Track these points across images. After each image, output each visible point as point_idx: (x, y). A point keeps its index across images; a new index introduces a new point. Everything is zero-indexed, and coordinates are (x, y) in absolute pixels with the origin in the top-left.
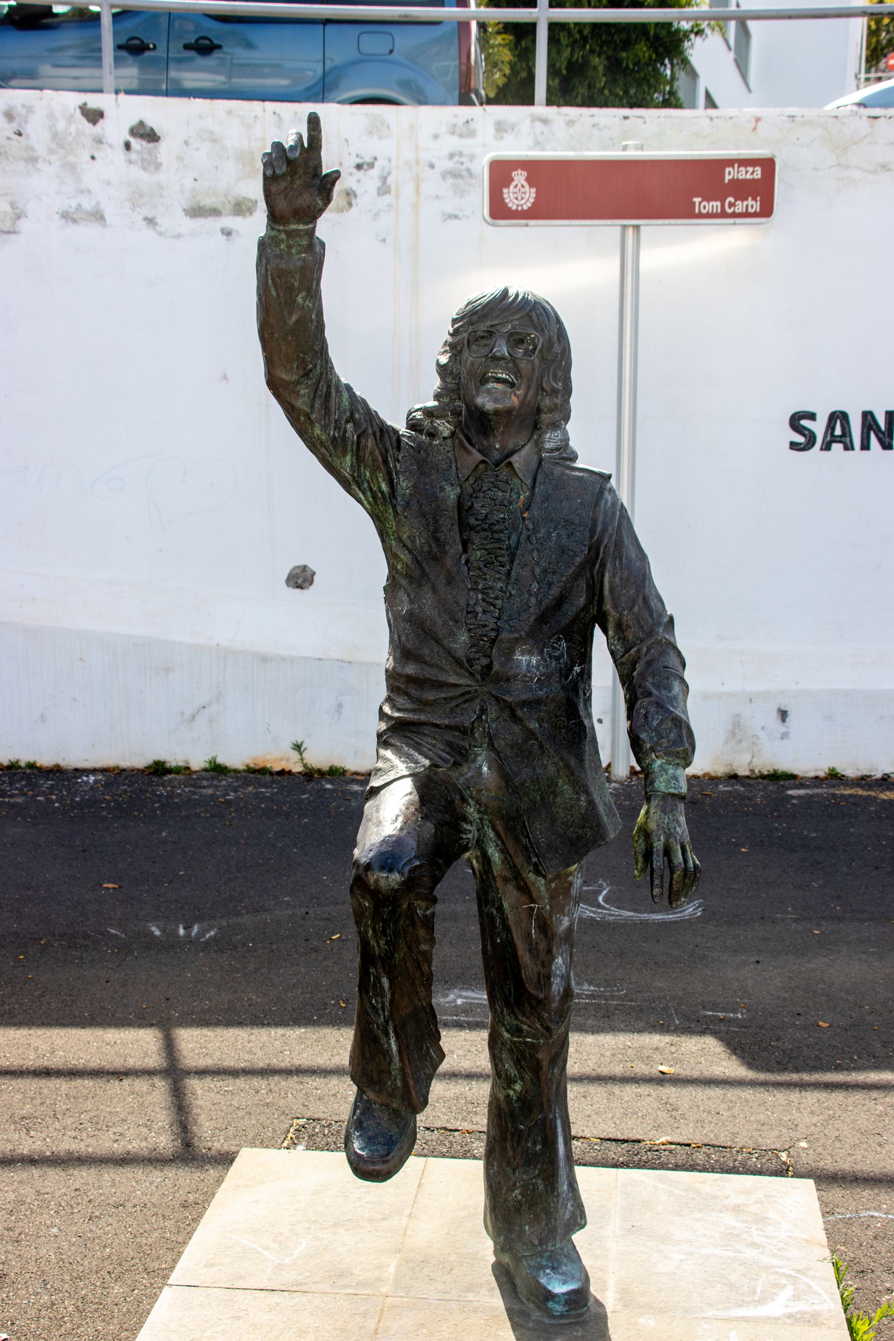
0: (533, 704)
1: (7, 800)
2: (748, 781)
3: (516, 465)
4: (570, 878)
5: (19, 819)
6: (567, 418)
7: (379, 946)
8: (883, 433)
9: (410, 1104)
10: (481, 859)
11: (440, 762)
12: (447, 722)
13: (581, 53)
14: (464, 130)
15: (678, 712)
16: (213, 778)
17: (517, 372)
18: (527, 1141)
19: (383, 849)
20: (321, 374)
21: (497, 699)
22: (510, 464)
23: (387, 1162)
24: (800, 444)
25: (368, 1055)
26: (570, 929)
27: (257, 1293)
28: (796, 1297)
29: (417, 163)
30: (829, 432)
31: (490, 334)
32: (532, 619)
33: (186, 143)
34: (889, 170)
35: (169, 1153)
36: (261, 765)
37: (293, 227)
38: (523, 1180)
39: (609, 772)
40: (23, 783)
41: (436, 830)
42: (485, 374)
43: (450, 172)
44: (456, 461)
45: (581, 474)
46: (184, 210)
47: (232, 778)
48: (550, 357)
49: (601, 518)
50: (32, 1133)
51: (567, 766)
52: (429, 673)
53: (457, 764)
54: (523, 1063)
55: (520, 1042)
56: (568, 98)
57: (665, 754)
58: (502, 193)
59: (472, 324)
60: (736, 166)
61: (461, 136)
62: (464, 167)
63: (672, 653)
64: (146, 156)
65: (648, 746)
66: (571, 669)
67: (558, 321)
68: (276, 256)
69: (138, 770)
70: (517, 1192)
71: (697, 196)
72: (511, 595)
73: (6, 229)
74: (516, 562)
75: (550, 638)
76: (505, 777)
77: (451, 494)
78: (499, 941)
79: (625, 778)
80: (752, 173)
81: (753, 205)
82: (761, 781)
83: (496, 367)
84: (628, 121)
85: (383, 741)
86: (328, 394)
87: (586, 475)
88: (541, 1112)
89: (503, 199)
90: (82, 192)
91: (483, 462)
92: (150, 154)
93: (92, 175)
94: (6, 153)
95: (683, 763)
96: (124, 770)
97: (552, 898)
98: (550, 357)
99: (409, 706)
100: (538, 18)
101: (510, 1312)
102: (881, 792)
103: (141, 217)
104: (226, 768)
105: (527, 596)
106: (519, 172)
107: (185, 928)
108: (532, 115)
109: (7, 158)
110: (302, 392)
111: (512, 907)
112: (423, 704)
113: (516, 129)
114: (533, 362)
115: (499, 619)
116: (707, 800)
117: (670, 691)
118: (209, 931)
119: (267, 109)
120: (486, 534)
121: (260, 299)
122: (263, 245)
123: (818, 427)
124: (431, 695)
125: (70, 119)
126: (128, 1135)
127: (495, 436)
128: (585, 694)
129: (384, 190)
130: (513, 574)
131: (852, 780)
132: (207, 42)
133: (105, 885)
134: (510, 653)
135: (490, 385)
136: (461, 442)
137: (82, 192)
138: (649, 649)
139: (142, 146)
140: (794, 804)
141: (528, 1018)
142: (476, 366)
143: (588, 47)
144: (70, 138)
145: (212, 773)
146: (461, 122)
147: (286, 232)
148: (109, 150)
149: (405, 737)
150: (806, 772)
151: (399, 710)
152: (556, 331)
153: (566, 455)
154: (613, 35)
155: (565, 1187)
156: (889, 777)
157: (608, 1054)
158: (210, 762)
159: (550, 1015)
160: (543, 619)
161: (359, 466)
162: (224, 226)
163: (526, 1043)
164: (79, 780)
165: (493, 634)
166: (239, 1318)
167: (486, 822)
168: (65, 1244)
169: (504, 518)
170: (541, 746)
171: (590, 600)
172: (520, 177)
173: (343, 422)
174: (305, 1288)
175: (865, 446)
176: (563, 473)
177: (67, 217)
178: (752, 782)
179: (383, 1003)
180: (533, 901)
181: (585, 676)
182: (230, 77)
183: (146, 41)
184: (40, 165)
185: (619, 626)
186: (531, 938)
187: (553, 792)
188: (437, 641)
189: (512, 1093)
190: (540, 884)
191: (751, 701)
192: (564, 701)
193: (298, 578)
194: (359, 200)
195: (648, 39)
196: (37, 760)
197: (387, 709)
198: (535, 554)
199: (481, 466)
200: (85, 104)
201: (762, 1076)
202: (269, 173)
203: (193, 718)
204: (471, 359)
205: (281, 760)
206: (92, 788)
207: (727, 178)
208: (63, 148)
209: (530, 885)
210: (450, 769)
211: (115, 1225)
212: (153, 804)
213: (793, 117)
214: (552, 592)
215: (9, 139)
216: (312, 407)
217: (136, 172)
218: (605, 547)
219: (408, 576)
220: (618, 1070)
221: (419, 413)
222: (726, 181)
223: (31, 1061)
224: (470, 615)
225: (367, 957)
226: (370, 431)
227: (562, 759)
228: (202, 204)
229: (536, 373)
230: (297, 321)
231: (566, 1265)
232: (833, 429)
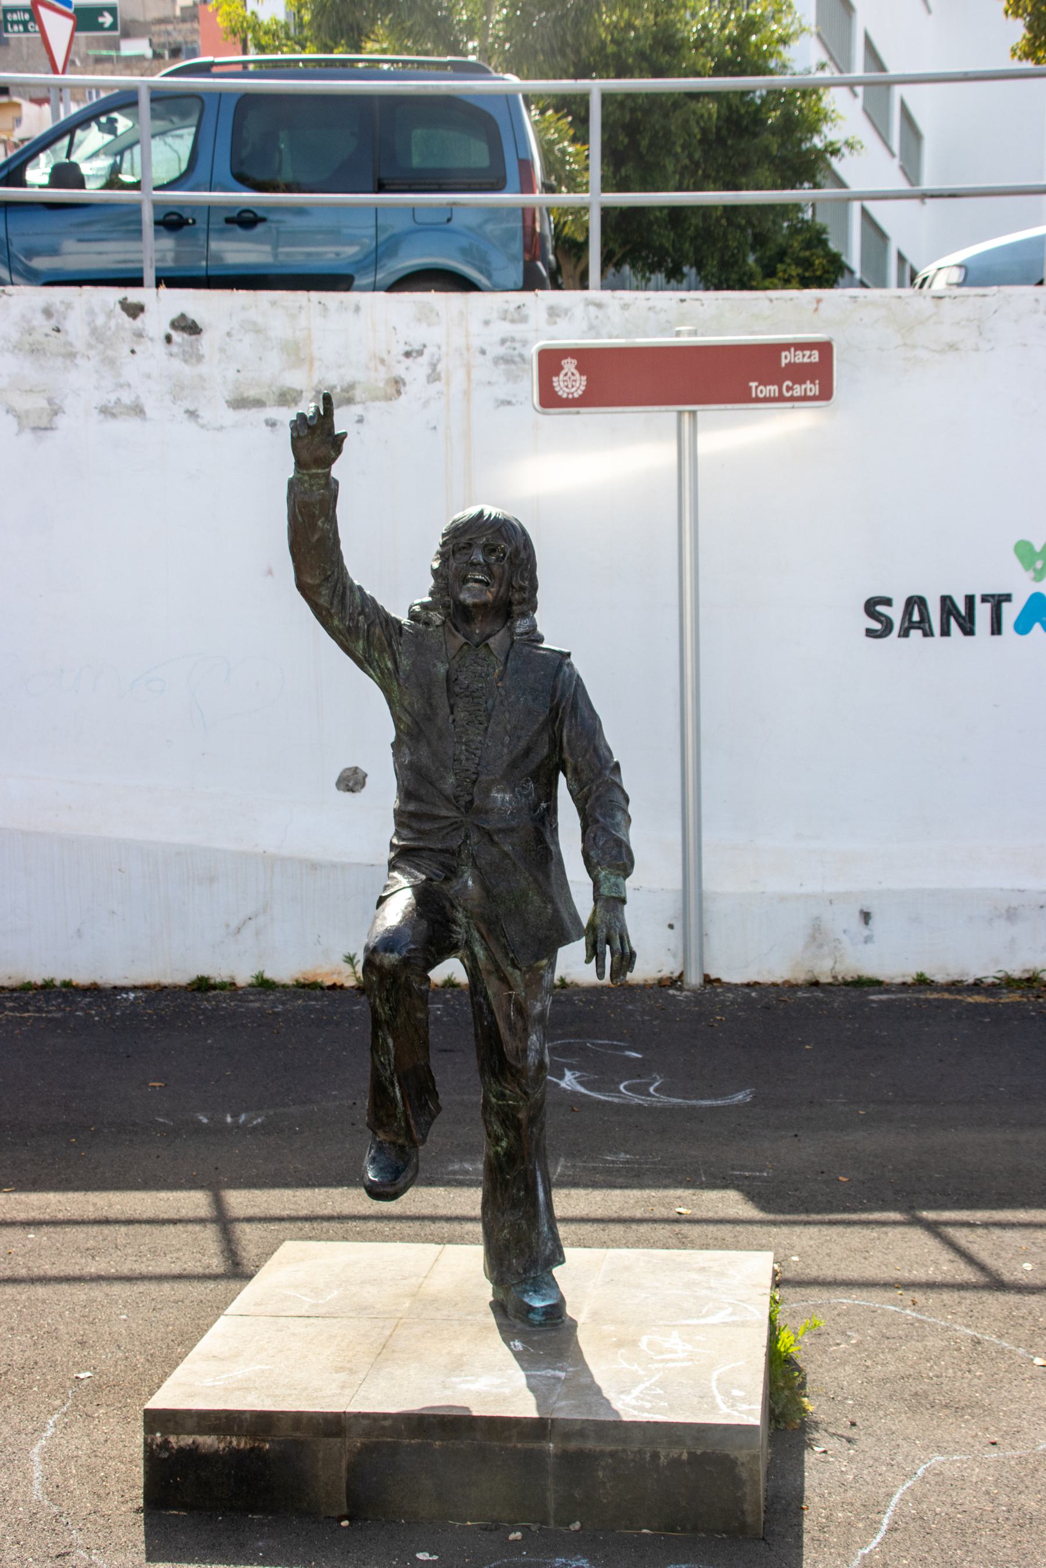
0: (508, 831)
1: (44, 1015)
2: (831, 988)
3: (492, 646)
4: (541, 971)
5: (59, 1031)
6: (534, 609)
7: (384, 1012)
8: (963, 618)
9: (411, 1140)
10: (470, 958)
11: (434, 877)
12: (439, 846)
13: (692, 181)
14: (516, 316)
15: (620, 835)
16: (259, 993)
17: (491, 575)
18: (513, 1188)
19: (386, 935)
20: (338, 578)
21: (478, 827)
22: (487, 645)
23: (395, 1185)
24: (877, 631)
25: (379, 1104)
26: (542, 1014)
27: (297, 1319)
28: (733, 1314)
29: (468, 349)
30: (907, 617)
31: (469, 545)
32: (505, 765)
33: (229, 334)
34: (957, 349)
35: (221, 1270)
36: (312, 979)
37: (314, 471)
38: (510, 1221)
39: (682, 981)
40: (60, 1000)
41: (429, 925)
42: (466, 576)
43: (502, 358)
44: (446, 643)
45: (545, 652)
46: (227, 402)
47: (280, 993)
48: (517, 562)
49: (560, 686)
50: (97, 1259)
51: (536, 880)
52: (425, 808)
53: (447, 879)
54: (507, 1123)
55: (504, 1105)
56: (812, 117)
57: (609, 867)
58: (552, 382)
59: (456, 538)
60: (792, 350)
61: (513, 321)
62: (516, 352)
63: (616, 790)
64: (187, 349)
65: (595, 861)
66: (538, 804)
67: (524, 533)
68: (301, 492)
69: (180, 987)
70: (505, 1231)
71: (754, 381)
72: (488, 746)
73: (43, 426)
74: (492, 721)
75: (520, 780)
76: (487, 891)
77: (442, 669)
78: (486, 1023)
79: (698, 986)
80: (810, 357)
81: (812, 388)
82: (844, 987)
83: (475, 570)
84: (685, 304)
85: (392, 866)
86: (344, 594)
87: (548, 653)
88: (523, 1164)
89: (553, 387)
90: (121, 386)
91: (466, 644)
92: (192, 346)
93: (131, 369)
94: (44, 349)
95: (623, 873)
96: (166, 987)
97: (527, 986)
98: (517, 562)
99: (411, 835)
100: (590, 203)
101: (500, 1326)
102: (969, 996)
103: (182, 410)
104: (274, 983)
105: (500, 747)
106: (569, 360)
107: (232, 1117)
108: (586, 299)
109: (45, 354)
110: (323, 592)
111: (495, 994)
112: (421, 834)
113: (569, 314)
114: (503, 566)
115: (478, 765)
116: (782, 1006)
117: (613, 819)
118: (256, 1119)
119: (311, 299)
120: (468, 699)
121: (290, 524)
122: (291, 484)
123: (895, 613)
124: (427, 826)
125: (110, 314)
126: (184, 1259)
127: (475, 624)
128: (551, 826)
129: (434, 376)
130: (490, 730)
131: (942, 985)
132: (251, 215)
133: (151, 1084)
134: (487, 792)
135: (470, 585)
136: (449, 629)
137: (121, 386)
138: (598, 788)
139: (183, 338)
140: (873, 1008)
141: (509, 1084)
142: (459, 570)
143: (700, 172)
144: (109, 333)
145: (259, 989)
146: (512, 307)
147: (309, 475)
148: (149, 343)
149: (409, 861)
150: (893, 978)
151: (403, 840)
152: (522, 542)
153: (534, 638)
154: (730, 159)
155: (546, 1229)
156: (982, 982)
157: (632, 1201)
158: (257, 978)
159: (527, 1081)
160: (513, 765)
161: (369, 649)
162: (268, 417)
163: (509, 1105)
164: (119, 997)
165: (474, 777)
166: (282, 1331)
167: (472, 926)
168: (134, 1326)
169: (482, 687)
170: (514, 864)
171: (552, 750)
172: (569, 365)
173: (356, 615)
174: (336, 1315)
175: (945, 632)
176: (530, 652)
177: (106, 411)
178: (834, 989)
179: (389, 1060)
180: (511, 989)
181: (551, 811)
182: (276, 246)
183: (185, 216)
184: (79, 360)
185: (576, 771)
186: (510, 1020)
187: (525, 902)
188: (431, 783)
189: (499, 1149)
190: (516, 976)
191: (831, 903)
192: (533, 830)
193: (349, 781)
194: (408, 388)
195: (772, 162)
196: (73, 978)
197: (395, 841)
198: (507, 715)
199: (465, 647)
200: (125, 299)
201: (771, 1217)
202: (295, 435)
203: (239, 930)
204: (455, 565)
205: (333, 973)
206: (132, 1004)
207: (784, 362)
208: (102, 342)
209: (508, 976)
210: (442, 882)
211: (176, 1313)
212: (197, 1017)
213: (855, 297)
214: (521, 744)
215: (47, 335)
216: (332, 604)
217: (177, 365)
218: (564, 708)
219: (409, 734)
220: (638, 1214)
221: (418, 607)
222: (783, 365)
223: (91, 1213)
224: (456, 763)
225: (377, 1023)
226: (377, 621)
227: (531, 875)
228: (245, 395)
229: (507, 574)
230: (318, 540)
231: (545, 1289)
232: (911, 614)
